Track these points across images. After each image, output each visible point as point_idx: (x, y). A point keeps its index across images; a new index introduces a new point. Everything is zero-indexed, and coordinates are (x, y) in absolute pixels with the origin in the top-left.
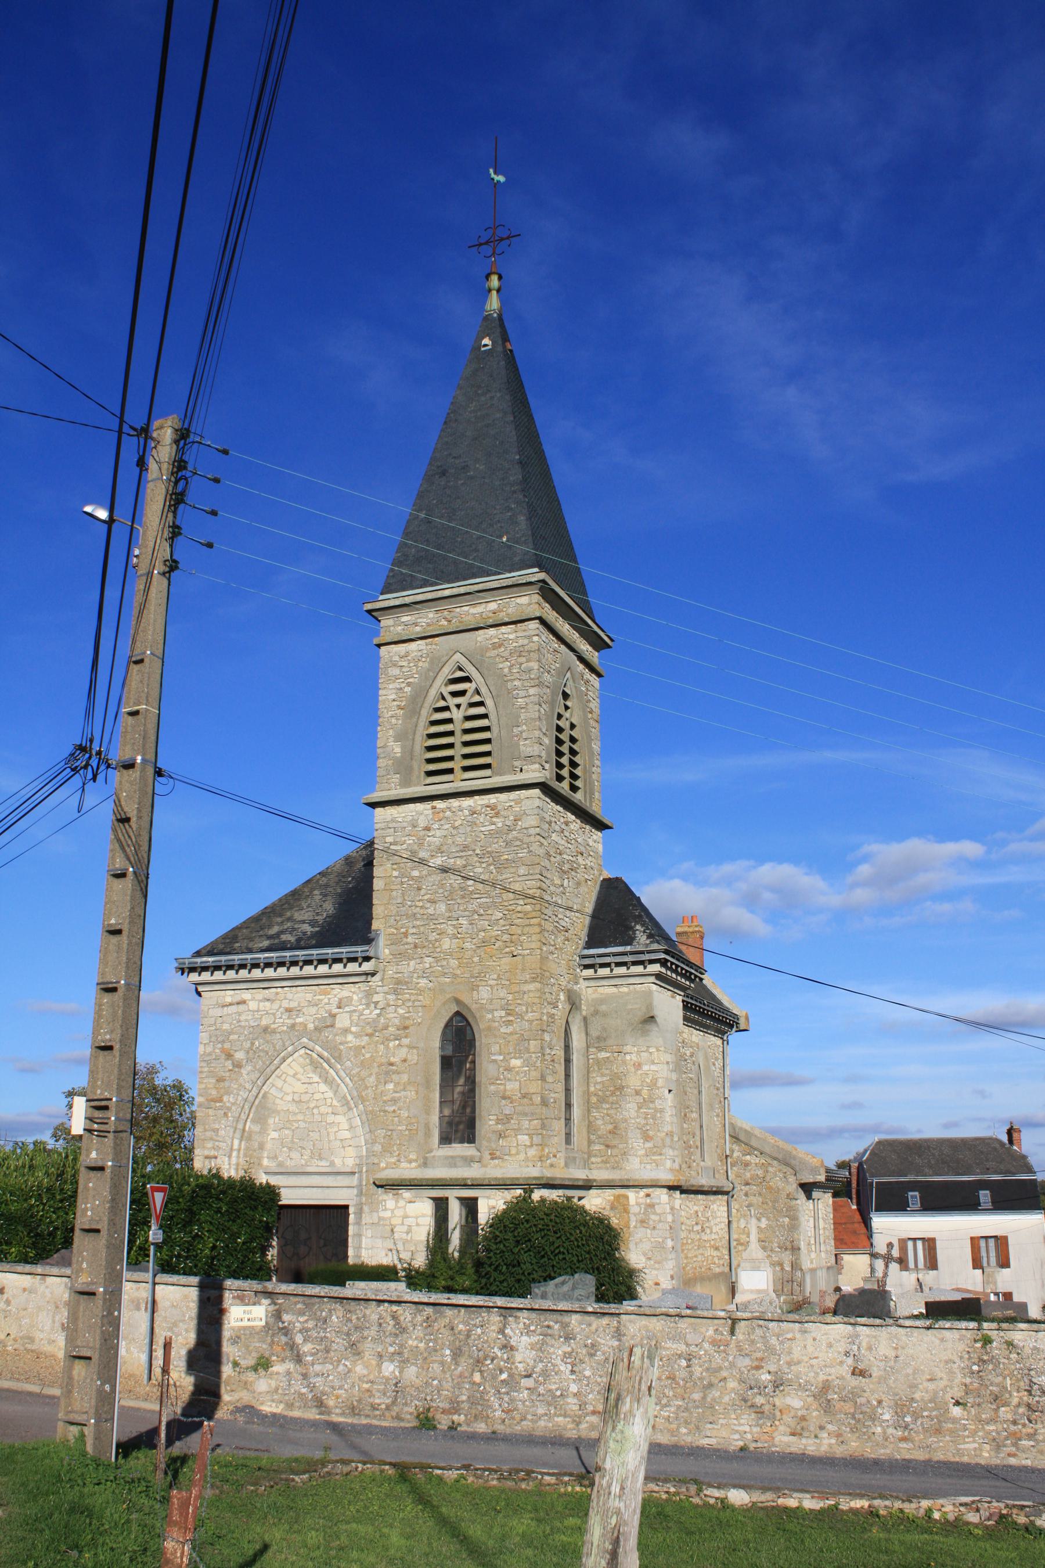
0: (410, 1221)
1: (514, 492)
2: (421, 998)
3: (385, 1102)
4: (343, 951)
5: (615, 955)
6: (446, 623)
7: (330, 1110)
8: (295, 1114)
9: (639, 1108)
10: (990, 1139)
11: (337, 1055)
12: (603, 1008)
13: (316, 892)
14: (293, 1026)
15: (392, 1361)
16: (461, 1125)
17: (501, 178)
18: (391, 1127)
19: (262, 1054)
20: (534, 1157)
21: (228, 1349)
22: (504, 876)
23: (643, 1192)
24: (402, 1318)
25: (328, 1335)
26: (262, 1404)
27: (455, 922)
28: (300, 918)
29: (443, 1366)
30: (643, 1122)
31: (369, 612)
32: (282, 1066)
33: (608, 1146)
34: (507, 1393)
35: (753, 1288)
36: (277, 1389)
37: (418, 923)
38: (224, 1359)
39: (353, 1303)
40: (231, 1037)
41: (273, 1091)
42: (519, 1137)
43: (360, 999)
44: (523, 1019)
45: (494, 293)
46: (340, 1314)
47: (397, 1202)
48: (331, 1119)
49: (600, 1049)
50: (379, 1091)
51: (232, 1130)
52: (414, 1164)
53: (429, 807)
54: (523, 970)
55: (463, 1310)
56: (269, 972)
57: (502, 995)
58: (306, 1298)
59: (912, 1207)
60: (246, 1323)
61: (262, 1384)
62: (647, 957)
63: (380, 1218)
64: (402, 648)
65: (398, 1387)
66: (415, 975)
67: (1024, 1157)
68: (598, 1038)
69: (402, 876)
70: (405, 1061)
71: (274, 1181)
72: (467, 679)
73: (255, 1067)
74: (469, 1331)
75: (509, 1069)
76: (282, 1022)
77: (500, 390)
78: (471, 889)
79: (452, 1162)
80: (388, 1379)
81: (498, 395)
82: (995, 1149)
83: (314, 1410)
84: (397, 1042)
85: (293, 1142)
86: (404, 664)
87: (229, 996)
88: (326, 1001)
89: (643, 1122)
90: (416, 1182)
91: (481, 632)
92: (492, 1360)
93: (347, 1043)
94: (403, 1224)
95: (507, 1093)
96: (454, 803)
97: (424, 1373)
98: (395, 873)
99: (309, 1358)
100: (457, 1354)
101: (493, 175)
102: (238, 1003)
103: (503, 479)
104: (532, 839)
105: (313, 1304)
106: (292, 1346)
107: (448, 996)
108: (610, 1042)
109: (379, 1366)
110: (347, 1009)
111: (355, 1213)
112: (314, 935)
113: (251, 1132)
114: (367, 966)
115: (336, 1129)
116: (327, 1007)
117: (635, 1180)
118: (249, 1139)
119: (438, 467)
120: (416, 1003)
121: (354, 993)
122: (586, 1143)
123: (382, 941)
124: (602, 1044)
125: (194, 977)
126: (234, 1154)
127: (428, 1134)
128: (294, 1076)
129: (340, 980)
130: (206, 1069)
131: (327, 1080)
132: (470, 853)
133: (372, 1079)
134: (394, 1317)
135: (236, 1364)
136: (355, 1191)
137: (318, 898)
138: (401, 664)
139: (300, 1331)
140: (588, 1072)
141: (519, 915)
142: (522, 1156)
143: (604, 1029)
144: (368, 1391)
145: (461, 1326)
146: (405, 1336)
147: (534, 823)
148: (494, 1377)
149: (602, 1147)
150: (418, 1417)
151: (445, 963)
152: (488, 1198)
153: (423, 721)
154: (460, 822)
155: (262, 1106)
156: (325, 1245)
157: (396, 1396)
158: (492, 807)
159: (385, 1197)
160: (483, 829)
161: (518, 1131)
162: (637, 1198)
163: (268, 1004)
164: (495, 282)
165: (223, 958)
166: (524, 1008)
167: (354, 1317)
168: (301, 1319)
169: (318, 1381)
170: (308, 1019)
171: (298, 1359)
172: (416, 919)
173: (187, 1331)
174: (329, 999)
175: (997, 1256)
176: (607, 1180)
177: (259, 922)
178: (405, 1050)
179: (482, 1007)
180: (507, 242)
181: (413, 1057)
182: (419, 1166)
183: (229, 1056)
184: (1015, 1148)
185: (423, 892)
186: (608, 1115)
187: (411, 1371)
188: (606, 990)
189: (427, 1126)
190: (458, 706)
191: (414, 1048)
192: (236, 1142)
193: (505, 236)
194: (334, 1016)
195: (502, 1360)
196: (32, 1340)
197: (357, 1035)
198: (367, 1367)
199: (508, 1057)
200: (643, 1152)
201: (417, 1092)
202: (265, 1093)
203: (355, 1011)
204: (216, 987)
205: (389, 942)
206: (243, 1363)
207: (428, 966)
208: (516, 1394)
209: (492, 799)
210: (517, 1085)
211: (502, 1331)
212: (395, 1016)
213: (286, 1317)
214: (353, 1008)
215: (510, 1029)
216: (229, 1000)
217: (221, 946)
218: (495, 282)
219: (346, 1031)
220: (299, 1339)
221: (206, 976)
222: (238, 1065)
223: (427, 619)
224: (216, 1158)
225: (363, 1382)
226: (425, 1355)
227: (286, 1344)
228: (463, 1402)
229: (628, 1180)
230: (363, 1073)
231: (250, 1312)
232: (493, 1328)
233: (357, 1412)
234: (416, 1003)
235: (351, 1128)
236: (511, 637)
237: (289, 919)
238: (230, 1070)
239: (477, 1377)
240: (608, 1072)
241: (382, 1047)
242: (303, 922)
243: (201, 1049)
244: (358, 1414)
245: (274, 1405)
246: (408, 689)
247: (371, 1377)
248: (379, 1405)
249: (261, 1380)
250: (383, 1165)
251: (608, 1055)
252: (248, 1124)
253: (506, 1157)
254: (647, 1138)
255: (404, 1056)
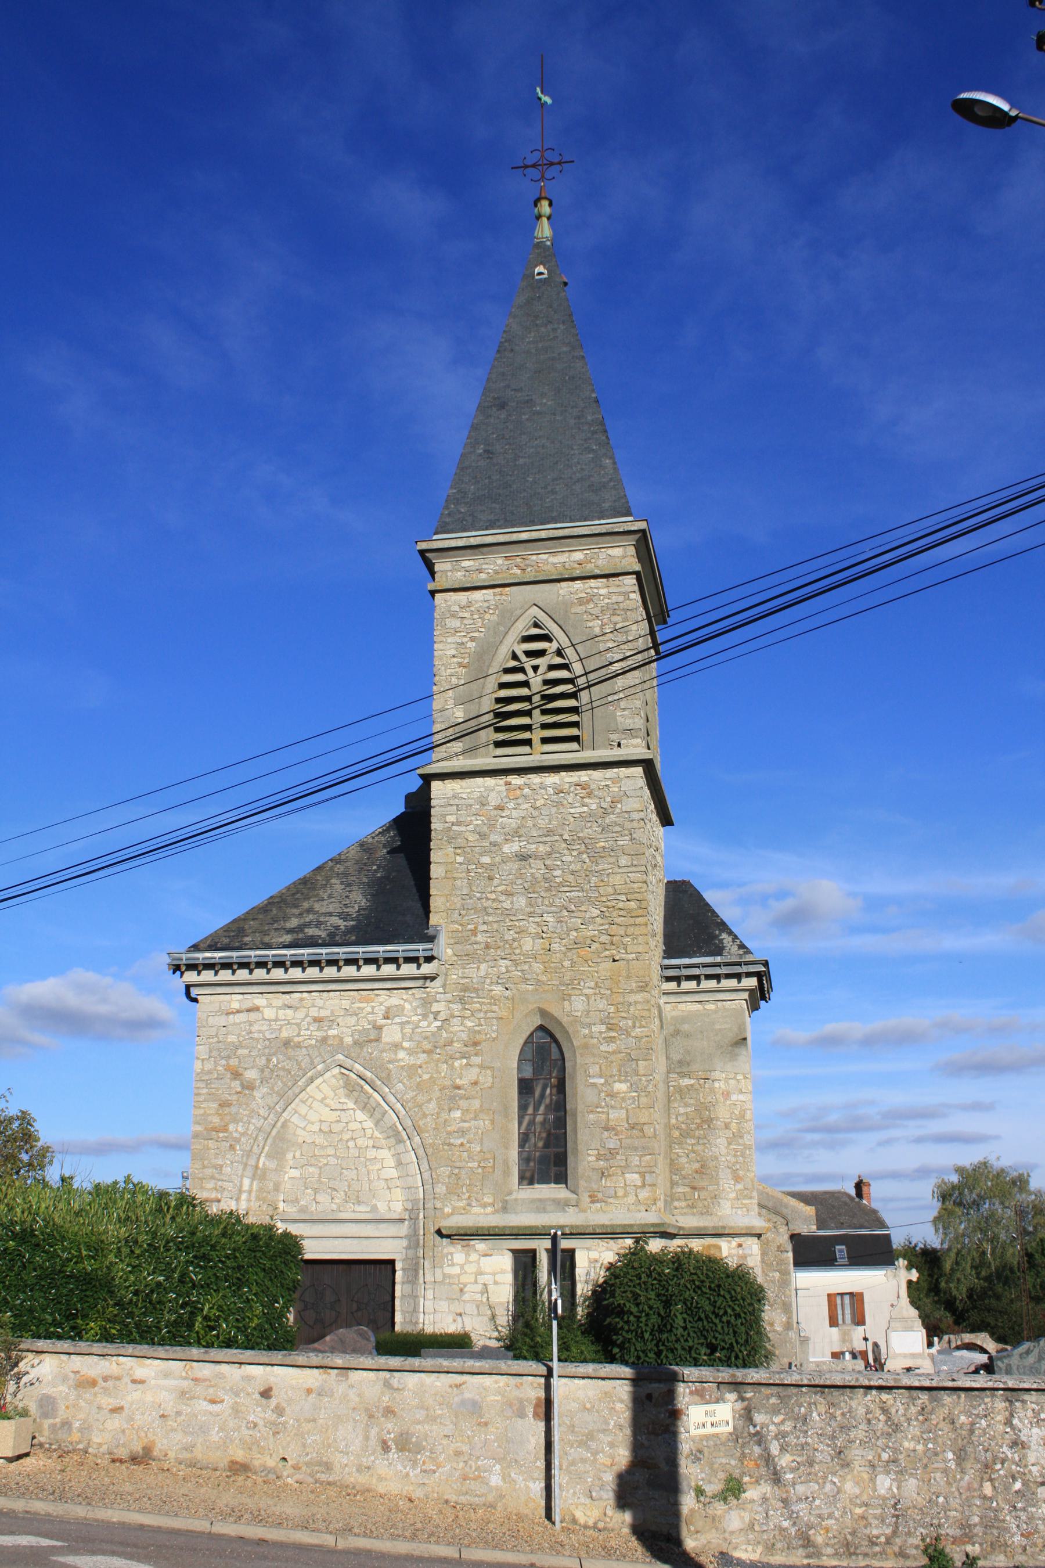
0: (487, 1279)
1: (594, 432)
2: (495, 1008)
3: (449, 1133)
4: (399, 949)
5: (705, 966)
6: (519, 572)
7: (371, 1143)
8: (323, 1148)
9: (729, 1144)
10: (839, 1192)
11: (384, 1075)
12: (686, 1027)
13: (333, 881)
14: (324, 1040)
15: (888, 1473)
16: (549, 1158)
17: (548, 100)
18: (458, 1164)
19: (282, 1073)
20: (647, 1199)
21: (690, 1471)
22: (600, 867)
23: (735, 1242)
24: (893, 1411)
25: (809, 1440)
26: (736, 1548)
27: (538, 919)
28: (323, 910)
29: (947, 1476)
30: (733, 1160)
31: (422, 552)
32: (308, 1089)
33: (694, 1188)
34: (1024, 1509)
35: (906, 1352)
36: (751, 1526)
37: (491, 919)
38: (684, 1485)
39: (836, 1393)
40: (240, 1052)
41: (295, 1119)
42: (627, 1175)
43: (415, 1009)
44: (628, 1035)
45: (545, 220)
46: (822, 1409)
47: (468, 1255)
48: (372, 1153)
49: (683, 1075)
50: (441, 1120)
51: (241, 1167)
52: (489, 1209)
53: (502, 782)
54: (628, 977)
55: (963, 1395)
56: (296, 973)
57: (601, 1007)
58: (780, 1389)
59: (840, 1261)
60: (709, 1430)
61: (735, 1519)
62: (745, 969)
63: (444, 1275)
64: (462, 597)
65: (897, 1509)
66: (488, 981)
67: (875, 1212)
68: (680, 1062)
69: (469, 862)
70: (476, 1083)
71: (294, 1229)
72: (546, 638)
73: (272, 1089)
74: (973, 1424)
75: (612, 1095)
76: (310, 1034)
77: (563, 322)
78: (558, 880)
79: (541, 1206)
80: (885, 1499)
81: (562, 327)
82: (846, 1204)
83: (801, 1552)
84: (465, 1061)
85: (319, 1181)
86: (466, 615)
87: (236, 1002)
88: (369, 1009)
89: (733, 1160)
90: (497, 1231)
91: (564, 584)
92: (1003, 1463)
93: (398, 1061)
94: (476, 1282)
95: (611, 1123)
96: (535, 779)
97: (926, 1487)
98: (459, 859)
99: (789, 1476)
100: (961, 1457)
101: (540, 95)
102: (248, 1011)
103: (579, 418)
104: (635, 824)
105: (790, 1397)
106: (768, 1459)
107: (531, 1007)
108: (694, 1067)
109: (873, 1480)
110: (397, 1020)
111: (403, 1269)
112: (349, 931)
113: (265, 1170)
114: (427, 969)
115: (379, 1166)
116: (370, 1017)
117: (731, 1228)
118: (263, 1178)
119: (495, 399)
120: (489, 1015)
121: (406, 1001)
122: (668, 1185)
123: (443, 939)
124: (685, 1069)
125: (191, 977)
126: (244, 1196)
127: (507, 1173)
128: (322, 1101)
129: (388, 985)
130: (205, 1091)
131: (365, 1106)
132: (557, 838)
133: (432, 1106)
134: (885, 1411)
135: (700, 1492)
136: (405, 1243)
137: (339, 887)
138: (461, 615)
139: (776, 1438)
140: (669, 1101)
141: (621, 913)
142: (631, 1199)
143: (688, 1052)
144: (863, 1517)
145: (963, 1418)
146: (899, 1435)
147: (637, 806)
148: (1007, 1488)
149: (687, 1189)
150: (925, 1551)
151: (526, 967)
152: (588, 1249)
153: (491, 683)
154: (542, 801)
155: (281, 1138)
156: (359, 1309)
157: (896, 1523)
158: (584, 786)
159: (451, 1249)
160: (572, 811)
161: (625, 1168)
162: (729, 1248)
163: (289, 1012)
164: (545, 208)
165: (235, 954)
166: (630, 1023)
167: (839, 1413)
168: (777, 1420)
169: (801, 1508)
170: (345, 1031)
171: (776, 1479)
172: (488, 914)
173: (612, 1445)
174: (373, 1007)
175: (853, 1314)
176: (697, 1228)
177: (272, 911)
178: (476, 1070)
179: (576, 1020)
180: (558, 168)
181: (486, 1079)
182: (496, 1211)
183: (236, 1075)
184: (864, 1202)
185: (496, 882)
186: (694, 1152)
187: (912, 1484)
188: (689, 1007)
189: (506, 1162)
190: (535, 668)
191: (488, 1068)
192: (246, 1182)
193: (556, 161)
194: (380, 1028)
195: (1014, 1462)
196: (328, 1467)
197: (410, 1052)
198: (858, 1483)
199: (610, 1080)
200: (733, 1195)
201: (493, 1122)
202: (286, 1121)
203: (408, 1022)
204: (219, 990)
205: (452, 941)
206: (710, 1489)
207: (504, 970)
208: (1034, 1510)
209: (583, 776)
210: (623, 1114)
211: (1008, 1422)
212: (460, 1029)
213: (759, 1418)
214: (404, 1019)
215: (612, 1047)
216: (236, 1006)
217: (226, 941)
218: (545, 208)
219: (396, 1046)
220: (774, 1448)
221: (208, 976)
222: (250, 1086)
223: (493, 566)
224: (219, 1201)
225: (856, 1505)
226: (925, 1461)
227: (761, 1456)
228: (975, 1525)
229: (724, 1227)
230: (419, 1097)
231: (713, 1413)
232: (999, 1418)
233: (852, 1550)
234: (489, 1015)
235: (399, 1164)
236: (603, 591)
237: (310, 911)
238: (238, 1093)
239: (988, 1489)
240: (692, 1101)
241: (445, 1066)
242: (331, 914)
243: (198, 1066)
244: (854, 1553)
245: (750, 1548)
246: (471, 645)
247: (865, 1498)
248: (878, 1537)
249: (732, 1513)
250: (447, 1210)
251: (692, 1082)
252: (262, 1159)
253: (611, 1200)
254: (737, 1179)
255: (475, 1078)
